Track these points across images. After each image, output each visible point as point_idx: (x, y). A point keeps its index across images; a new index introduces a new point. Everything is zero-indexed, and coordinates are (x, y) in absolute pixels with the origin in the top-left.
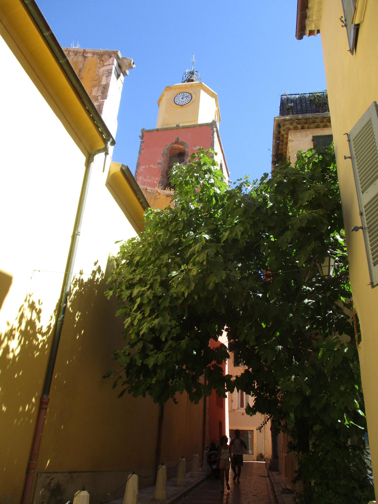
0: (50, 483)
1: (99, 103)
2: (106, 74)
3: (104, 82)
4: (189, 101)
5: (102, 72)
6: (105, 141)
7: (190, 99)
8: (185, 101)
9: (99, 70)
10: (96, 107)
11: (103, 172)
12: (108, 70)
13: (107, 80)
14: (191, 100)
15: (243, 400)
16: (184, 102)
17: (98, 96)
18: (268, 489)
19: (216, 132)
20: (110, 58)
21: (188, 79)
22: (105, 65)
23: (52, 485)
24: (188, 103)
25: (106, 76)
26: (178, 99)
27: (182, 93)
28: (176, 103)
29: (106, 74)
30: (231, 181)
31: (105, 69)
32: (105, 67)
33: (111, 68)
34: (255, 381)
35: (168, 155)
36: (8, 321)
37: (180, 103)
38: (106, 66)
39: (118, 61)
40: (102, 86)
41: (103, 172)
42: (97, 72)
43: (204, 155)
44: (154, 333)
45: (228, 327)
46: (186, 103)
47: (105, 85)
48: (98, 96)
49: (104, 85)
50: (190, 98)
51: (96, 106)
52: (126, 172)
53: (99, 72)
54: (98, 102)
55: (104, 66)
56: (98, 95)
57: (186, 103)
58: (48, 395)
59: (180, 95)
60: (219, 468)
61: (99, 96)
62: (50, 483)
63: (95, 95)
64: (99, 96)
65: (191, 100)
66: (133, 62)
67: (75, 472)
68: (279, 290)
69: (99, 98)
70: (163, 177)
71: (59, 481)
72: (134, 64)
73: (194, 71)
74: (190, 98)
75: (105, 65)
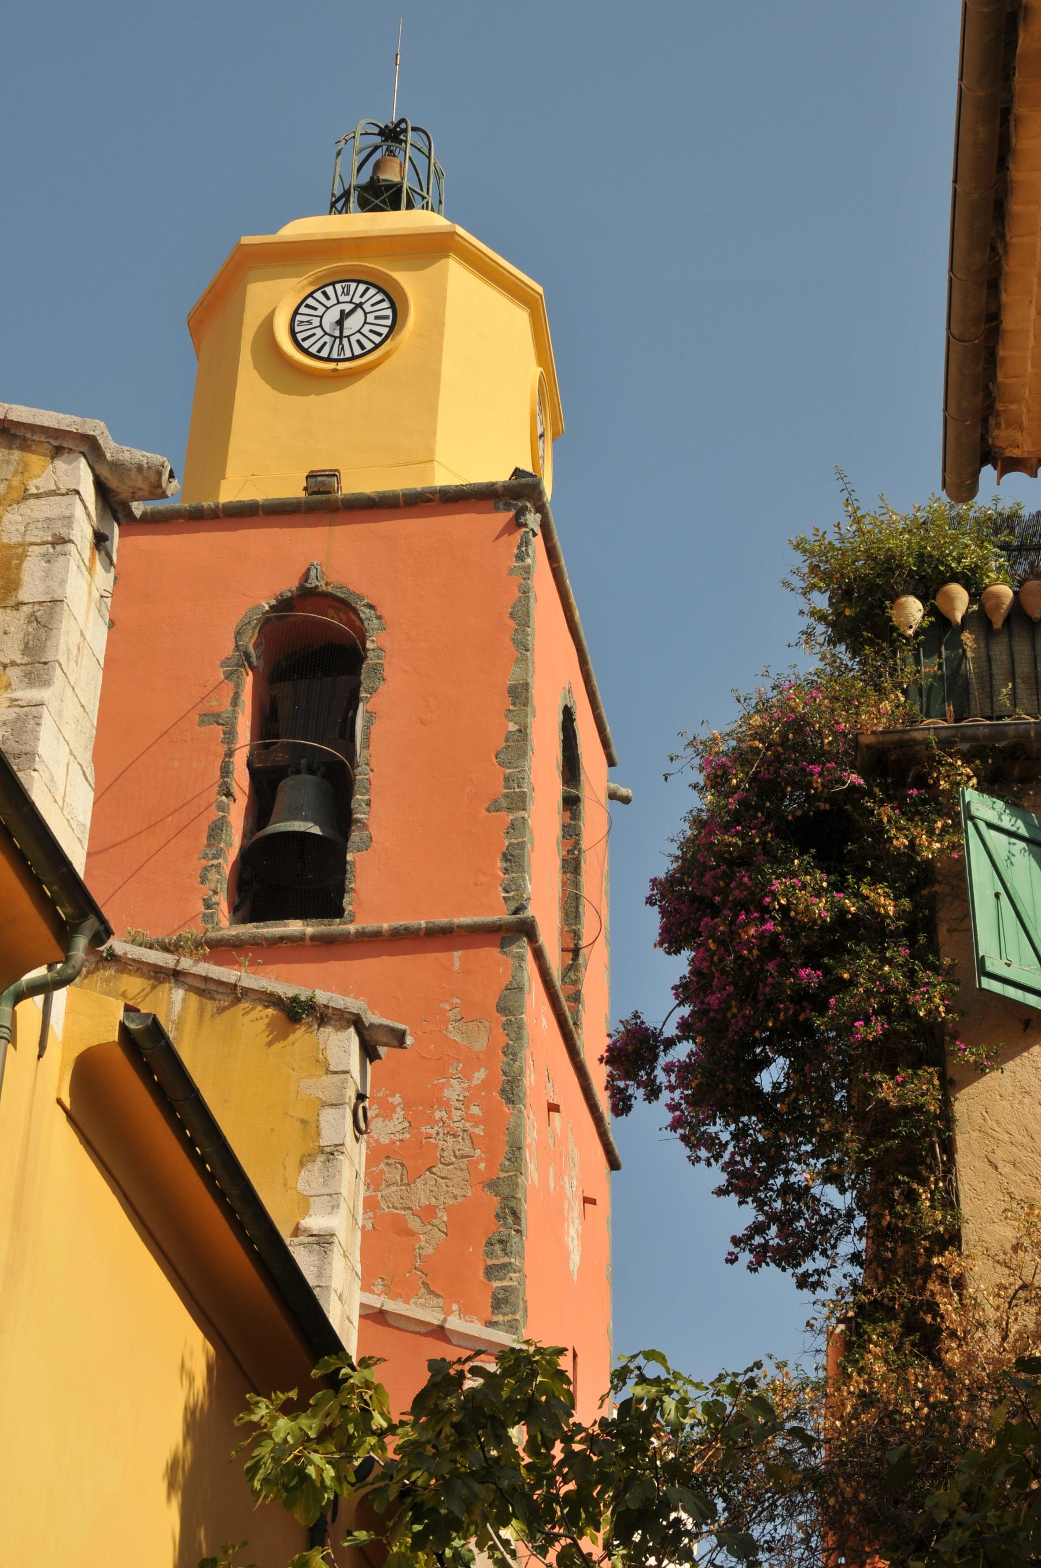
2: (44, 543)
3: (31, 589)
6: (64, 934)
7: (388, 322)
11: (40, 1056)
13: (48, 575)
15: (536, 281)
18: (412, 1332)
19: (540, 537)
22: (33, 491)
24: (377, 346)
27: (338, 286)
28: (306, 344)
29: (44, 543)
30: (624, 791)
31: (39, 515)
33: (67, 513)
38: (37, 496)
41: (40, 1056)
46: (362, 347)
47: (41, 603)
50: (386, 317)
52: (145, 1043)
56: (8, 661)
57: (362, 347)
59: (325, 294)
61: (13, 664)
66: (171, 472)
72: (171, 475)
73: (403, 126)
74: (386, 317)
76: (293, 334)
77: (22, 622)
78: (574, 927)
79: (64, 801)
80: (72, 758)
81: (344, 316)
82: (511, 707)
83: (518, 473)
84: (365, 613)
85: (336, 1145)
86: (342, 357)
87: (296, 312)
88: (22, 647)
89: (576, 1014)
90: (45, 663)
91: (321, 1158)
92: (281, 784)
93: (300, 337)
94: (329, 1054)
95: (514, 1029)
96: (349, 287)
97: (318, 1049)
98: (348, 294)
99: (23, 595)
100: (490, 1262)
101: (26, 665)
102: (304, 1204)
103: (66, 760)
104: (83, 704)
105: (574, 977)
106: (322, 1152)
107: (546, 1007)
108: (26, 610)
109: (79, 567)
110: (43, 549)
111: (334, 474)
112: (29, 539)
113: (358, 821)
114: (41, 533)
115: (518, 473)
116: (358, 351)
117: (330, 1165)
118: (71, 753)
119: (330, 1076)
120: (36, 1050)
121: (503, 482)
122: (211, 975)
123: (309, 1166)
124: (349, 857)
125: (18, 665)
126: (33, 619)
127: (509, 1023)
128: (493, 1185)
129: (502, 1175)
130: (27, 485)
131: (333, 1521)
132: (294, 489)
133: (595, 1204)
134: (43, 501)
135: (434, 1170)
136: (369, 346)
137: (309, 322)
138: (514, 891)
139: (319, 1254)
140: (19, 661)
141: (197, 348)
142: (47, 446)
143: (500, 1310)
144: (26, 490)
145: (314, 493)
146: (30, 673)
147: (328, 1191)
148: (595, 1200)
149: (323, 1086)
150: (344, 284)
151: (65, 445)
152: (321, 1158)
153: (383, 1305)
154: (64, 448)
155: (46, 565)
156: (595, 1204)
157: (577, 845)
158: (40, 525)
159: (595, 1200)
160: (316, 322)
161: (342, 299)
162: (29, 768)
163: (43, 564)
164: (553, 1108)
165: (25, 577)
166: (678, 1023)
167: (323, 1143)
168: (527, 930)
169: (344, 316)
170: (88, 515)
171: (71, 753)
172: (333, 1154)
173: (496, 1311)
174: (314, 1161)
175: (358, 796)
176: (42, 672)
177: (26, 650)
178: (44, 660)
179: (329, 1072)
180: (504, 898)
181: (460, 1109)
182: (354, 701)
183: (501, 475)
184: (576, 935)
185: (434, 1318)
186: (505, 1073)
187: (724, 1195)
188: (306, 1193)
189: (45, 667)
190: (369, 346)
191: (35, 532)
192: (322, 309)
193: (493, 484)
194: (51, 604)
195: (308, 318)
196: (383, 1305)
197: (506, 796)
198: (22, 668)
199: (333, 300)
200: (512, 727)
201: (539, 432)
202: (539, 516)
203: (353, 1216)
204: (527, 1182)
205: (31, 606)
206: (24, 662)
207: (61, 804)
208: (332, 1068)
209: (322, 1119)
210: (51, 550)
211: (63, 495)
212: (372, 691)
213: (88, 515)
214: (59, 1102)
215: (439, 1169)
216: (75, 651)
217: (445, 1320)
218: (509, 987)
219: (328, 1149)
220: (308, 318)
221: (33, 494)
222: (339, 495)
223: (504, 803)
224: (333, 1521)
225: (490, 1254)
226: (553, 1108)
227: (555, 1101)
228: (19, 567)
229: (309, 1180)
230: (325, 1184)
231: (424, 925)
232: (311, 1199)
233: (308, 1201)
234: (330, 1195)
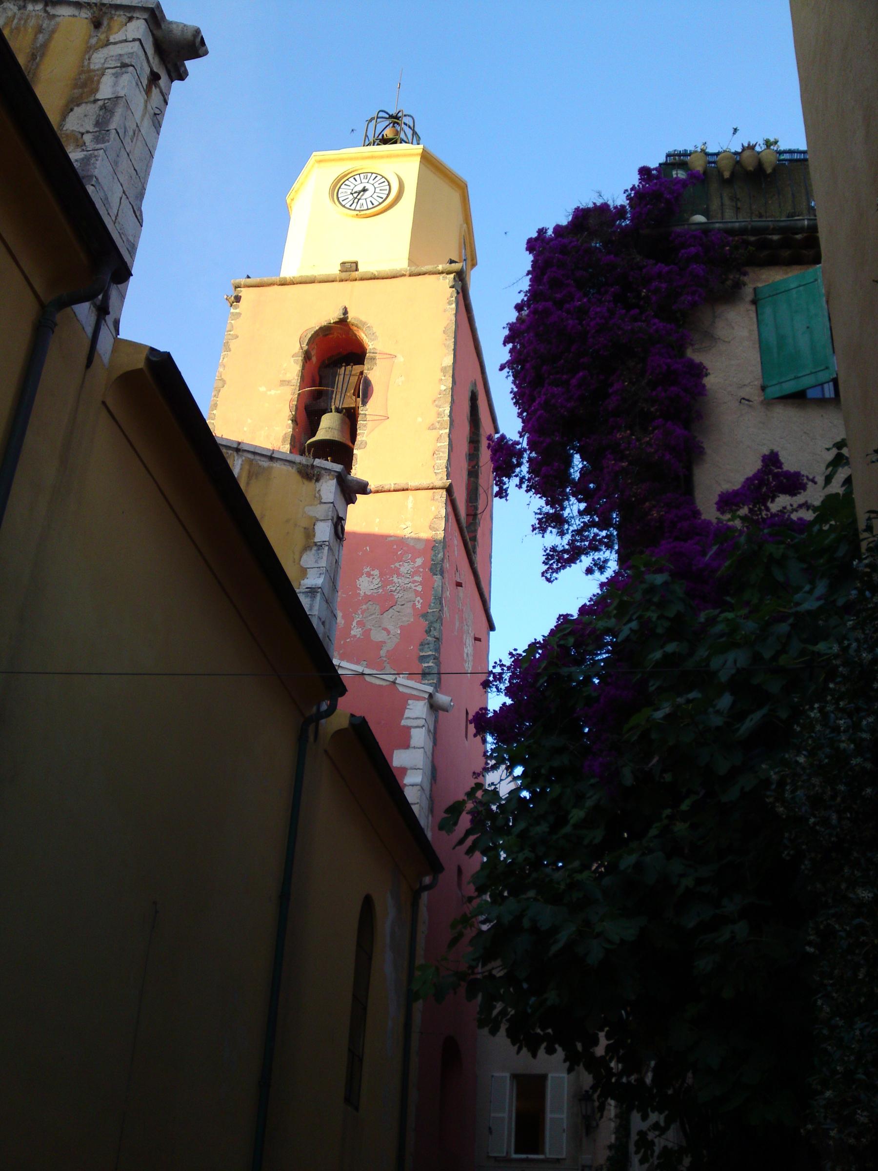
1: (85, 153)
4: (381, 200)
5: (103, 61)
8: (371, 199)
9: (94, 56)
16: (368, 200)
17: (82, 134)
21: (380, 137)
22: (112, 40)
24: (380, 204)
25: (113, 74)
28: (343, 203)
32: (111, 47)
35: (314, 359)
38: (115, 43)
39: (155, 32)
40: (100, 103)
42: (86, 63)
44: (865, 531)
45: (666, 1112)
47: (109, 99)
48: (82, 134)
49: (105, 99)
50: (386, 190)
51: (76, 161)
53: (92, 61)
54: (83, 150)
55: (107, 43)
60: (410, 702)
61: (88, 132)
63: (74, 128)
64: (88, 132)
69: (87, 138)
70: (297, 424)
75: (112, 40)
77: (96, 109)
78: (474, 504)
79: (116, 219)
82: (443, 378)
85: (324, 542)
86: (362, 209)
88: (94, 123)
89: (474, 547)
90: (108, 131)
91: (315, 548)
94: (322, 493)
96: (367, 176)
97: (316, 490)
98: (366, 178)
99: (99, 96)
100: (422, 654)
101: (96, 132)
103: (120, 195)
104: (136, 168)
105: (473, 529)
106: (316, 545)
109: (137, 84)
110: (113, 71)
112: (106, 66)
114: (114, 62)
116: (370, 206)
117: (319, 552)
118: (124, 192)
119: (322, 505)
123: (308, 552)
124: (355, 452)
125: (91, 133)
126: (103, 107)
130: (109, 38)
133: (480, 641)
134: (117, 46)
136: (376, 203)
139: (311, 597)
140: (91, 131)
142: (124, 17)
143: (426, 678)
144: (108, 40)
147: (318, 565)
148: (481, 639)
150: (364, 174)
151: (135, 15)
152: (315, 548)
153: (363, 671)
154: (134, 17)
155: (115, 79)
156: (480, 641)
158: (114, 58)
159: (481, 639)
161: (363, 181)
162: (89, 184)
164: (459, 584)
166: (542, 232)
171: (124, 192)
172: (322, 546)
173: (424, 679)
174: (311, 550)
176: (105, 136)
177: (97, 124)
178: (107, 129)
179: (321, 503)
181: (408, 578)
184: (476, 508)
187: (552, 630)
188: (305, 567)
189: (108, 133)
190: (376, 203)
191: (110, 62)
194: (116, 99)
195: (345, 190)
196: (363, 671)
198: (93, 134)
201: (464, 258)
203: (333, 583)
204: (443, 615)
205: (103, 101)
206: (94, 130)
207: (114, 219)
208: (323, 501)
209: (316, 527)
210: (119, 71)
211: (130, 41)
216: (131, 133)
218: (437, 517)
219: (319, 544)
220: (345, 190)
221: (112, 43)
223: (438, 426)
226: (459, 584)
228: (99, 82)
230: (316, 562)
232: (308, 570)
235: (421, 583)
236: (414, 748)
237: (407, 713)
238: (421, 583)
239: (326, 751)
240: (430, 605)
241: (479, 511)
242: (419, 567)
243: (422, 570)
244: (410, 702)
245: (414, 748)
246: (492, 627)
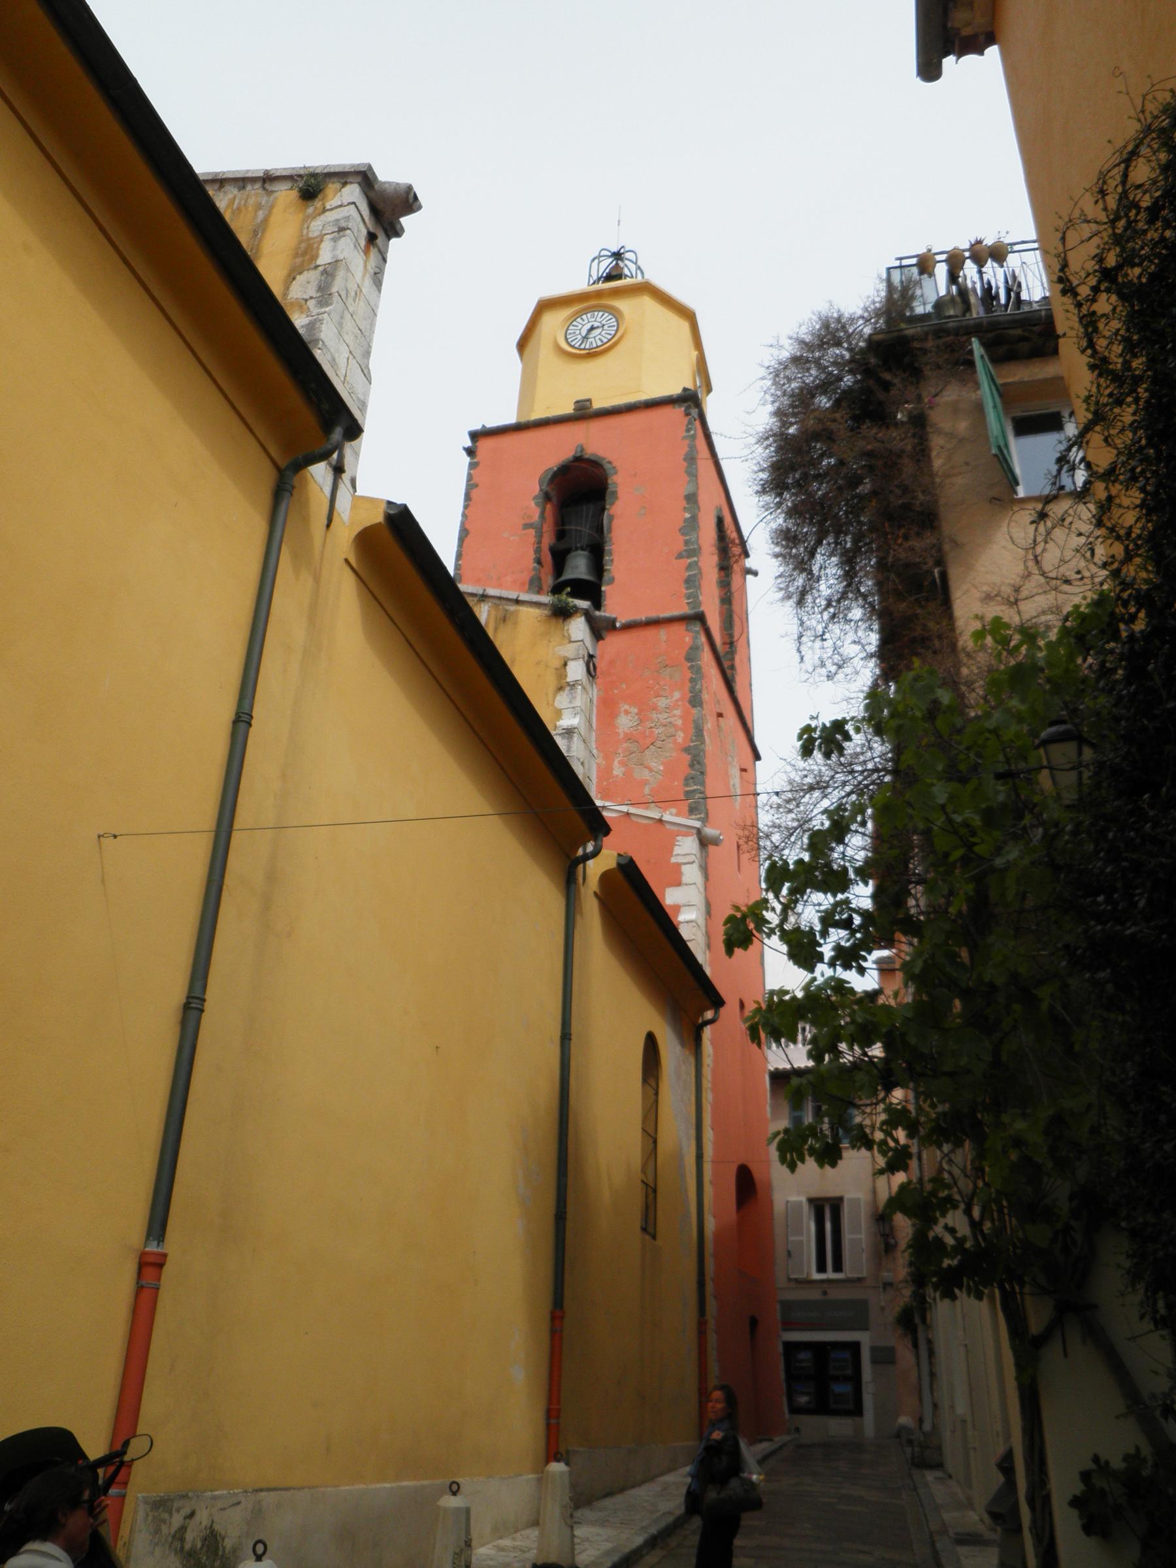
0: (183, 1529)
1: (310, 318)
2: (333, 233)
5: (321, 228)
9: (311, 225)
10: (301, 331)
12: (337, 220)
14: (617, 331)
15: (844, 1329)
17: (306, 300)
20: (343, 187)
22: (328, 207)
23: (190, 1536)
24: (609, 340)
25: (332, 239)
26: (580, 326)
29: (333, 233)
34: (792, 1156)
36: (521, 527)
37: (600, 316)
38: (332, 209)
39: (369, 194)
40: (321, 269)
41: (328, 526)
43: (1067, 322)
47: (329, 264)
49: (325, 265)
50: (614, 326)
51: (302, 327)
55: (324, 210)
58: (163, 1241)
62: (183, 1529)
64: (311, 298)
65: (617, 331)
67: (268, 1490)
68: (871, 929)
71: (213, 1522)
74: (614, 326)
75: (328, 207)
76: (566, 339)
80: (351, 357)
81: (592, 328)
83: (685, 390)
84: (607, 466)
87: (567, 329)
90: (330, 294)
91: (568, 688)
92: (569, 556)
93: (569, 340)
95: (697, 671)
99: (319, 262)
102: (558, 714)
103: (347, 355)
104: (361, 328)
107: (713, 663)
108: (321, 269)
111: (589, 400)
112: (324, 232)
113: (607, 570)
114: (331, 228)
115: (685, 390)
120: (325, 522)
121: (678, 395)
122: (502, 596)
124: (603, 588)
127: (692, 666)
128: (687, 750)
129: (692, 744)
131: (584, 883)
132: (569, 409)
135: (655, 744)
137: (574, 333)
138: (694, 599)
141: (521, 360)
144: (324, 208)
145: (580, 410)
146: (321, 301)
149: (569, 650)
153: (518, 597)
157: (729, 591)
160: (578, 332)
163: (332, 243)
164: (720, 715)
165: (321, 252)
167: (568, 680)
168: (700, 618)
169: (592, 328)
170: (363, 220)
171: (351, 352)
175: (607, 558)
179: (570, 642)
180: (687, 603)
182: (603, 509)
183: (675, 390)
184: (731, 636)
185: (657, 815)
186: (691, 692)
190: (605, 340)
192: (580, 326)
193: (672, 395)
196: (518, 597)
197: (686, 551)
199: (586, 321)
200: (687, 515)
202: (696, 410)
207: (343, 379)
208: (573, 639)
212: (612, 504)
213: (363, 220)
214: (346, 561)
215: (659, 743)
217: (662, 816)
219: (572, 683)
222: (591, 410)
224: (584, 883)
225: (687, 785)
227: (719, 711)
229: (562, 700)
231: (644, 619)
233: (561, 712)
234: (573, 708)
235: (681, 717)
236: (686, 884)
237: (677, 850)
238: (681, 717)
239: (346, 561)
240: (691, 739)
241: (736, 638)
242: (677, 701)
243: (680, 703)
244: (679, 838)
245: (686, 884)
246: (757, 757)
